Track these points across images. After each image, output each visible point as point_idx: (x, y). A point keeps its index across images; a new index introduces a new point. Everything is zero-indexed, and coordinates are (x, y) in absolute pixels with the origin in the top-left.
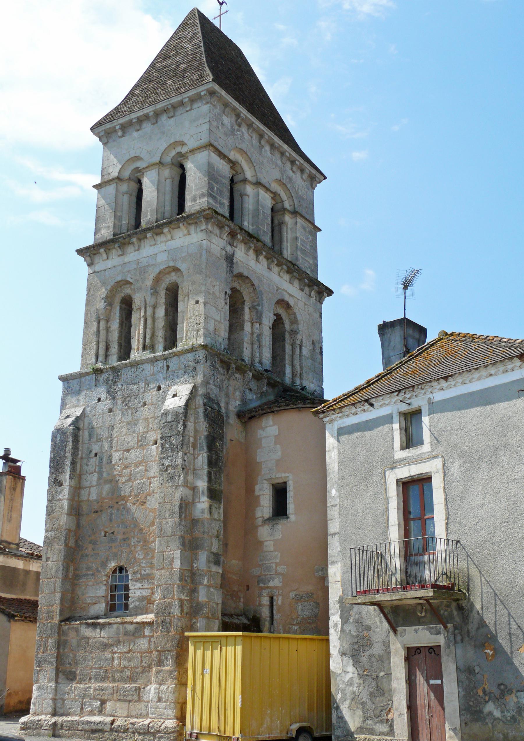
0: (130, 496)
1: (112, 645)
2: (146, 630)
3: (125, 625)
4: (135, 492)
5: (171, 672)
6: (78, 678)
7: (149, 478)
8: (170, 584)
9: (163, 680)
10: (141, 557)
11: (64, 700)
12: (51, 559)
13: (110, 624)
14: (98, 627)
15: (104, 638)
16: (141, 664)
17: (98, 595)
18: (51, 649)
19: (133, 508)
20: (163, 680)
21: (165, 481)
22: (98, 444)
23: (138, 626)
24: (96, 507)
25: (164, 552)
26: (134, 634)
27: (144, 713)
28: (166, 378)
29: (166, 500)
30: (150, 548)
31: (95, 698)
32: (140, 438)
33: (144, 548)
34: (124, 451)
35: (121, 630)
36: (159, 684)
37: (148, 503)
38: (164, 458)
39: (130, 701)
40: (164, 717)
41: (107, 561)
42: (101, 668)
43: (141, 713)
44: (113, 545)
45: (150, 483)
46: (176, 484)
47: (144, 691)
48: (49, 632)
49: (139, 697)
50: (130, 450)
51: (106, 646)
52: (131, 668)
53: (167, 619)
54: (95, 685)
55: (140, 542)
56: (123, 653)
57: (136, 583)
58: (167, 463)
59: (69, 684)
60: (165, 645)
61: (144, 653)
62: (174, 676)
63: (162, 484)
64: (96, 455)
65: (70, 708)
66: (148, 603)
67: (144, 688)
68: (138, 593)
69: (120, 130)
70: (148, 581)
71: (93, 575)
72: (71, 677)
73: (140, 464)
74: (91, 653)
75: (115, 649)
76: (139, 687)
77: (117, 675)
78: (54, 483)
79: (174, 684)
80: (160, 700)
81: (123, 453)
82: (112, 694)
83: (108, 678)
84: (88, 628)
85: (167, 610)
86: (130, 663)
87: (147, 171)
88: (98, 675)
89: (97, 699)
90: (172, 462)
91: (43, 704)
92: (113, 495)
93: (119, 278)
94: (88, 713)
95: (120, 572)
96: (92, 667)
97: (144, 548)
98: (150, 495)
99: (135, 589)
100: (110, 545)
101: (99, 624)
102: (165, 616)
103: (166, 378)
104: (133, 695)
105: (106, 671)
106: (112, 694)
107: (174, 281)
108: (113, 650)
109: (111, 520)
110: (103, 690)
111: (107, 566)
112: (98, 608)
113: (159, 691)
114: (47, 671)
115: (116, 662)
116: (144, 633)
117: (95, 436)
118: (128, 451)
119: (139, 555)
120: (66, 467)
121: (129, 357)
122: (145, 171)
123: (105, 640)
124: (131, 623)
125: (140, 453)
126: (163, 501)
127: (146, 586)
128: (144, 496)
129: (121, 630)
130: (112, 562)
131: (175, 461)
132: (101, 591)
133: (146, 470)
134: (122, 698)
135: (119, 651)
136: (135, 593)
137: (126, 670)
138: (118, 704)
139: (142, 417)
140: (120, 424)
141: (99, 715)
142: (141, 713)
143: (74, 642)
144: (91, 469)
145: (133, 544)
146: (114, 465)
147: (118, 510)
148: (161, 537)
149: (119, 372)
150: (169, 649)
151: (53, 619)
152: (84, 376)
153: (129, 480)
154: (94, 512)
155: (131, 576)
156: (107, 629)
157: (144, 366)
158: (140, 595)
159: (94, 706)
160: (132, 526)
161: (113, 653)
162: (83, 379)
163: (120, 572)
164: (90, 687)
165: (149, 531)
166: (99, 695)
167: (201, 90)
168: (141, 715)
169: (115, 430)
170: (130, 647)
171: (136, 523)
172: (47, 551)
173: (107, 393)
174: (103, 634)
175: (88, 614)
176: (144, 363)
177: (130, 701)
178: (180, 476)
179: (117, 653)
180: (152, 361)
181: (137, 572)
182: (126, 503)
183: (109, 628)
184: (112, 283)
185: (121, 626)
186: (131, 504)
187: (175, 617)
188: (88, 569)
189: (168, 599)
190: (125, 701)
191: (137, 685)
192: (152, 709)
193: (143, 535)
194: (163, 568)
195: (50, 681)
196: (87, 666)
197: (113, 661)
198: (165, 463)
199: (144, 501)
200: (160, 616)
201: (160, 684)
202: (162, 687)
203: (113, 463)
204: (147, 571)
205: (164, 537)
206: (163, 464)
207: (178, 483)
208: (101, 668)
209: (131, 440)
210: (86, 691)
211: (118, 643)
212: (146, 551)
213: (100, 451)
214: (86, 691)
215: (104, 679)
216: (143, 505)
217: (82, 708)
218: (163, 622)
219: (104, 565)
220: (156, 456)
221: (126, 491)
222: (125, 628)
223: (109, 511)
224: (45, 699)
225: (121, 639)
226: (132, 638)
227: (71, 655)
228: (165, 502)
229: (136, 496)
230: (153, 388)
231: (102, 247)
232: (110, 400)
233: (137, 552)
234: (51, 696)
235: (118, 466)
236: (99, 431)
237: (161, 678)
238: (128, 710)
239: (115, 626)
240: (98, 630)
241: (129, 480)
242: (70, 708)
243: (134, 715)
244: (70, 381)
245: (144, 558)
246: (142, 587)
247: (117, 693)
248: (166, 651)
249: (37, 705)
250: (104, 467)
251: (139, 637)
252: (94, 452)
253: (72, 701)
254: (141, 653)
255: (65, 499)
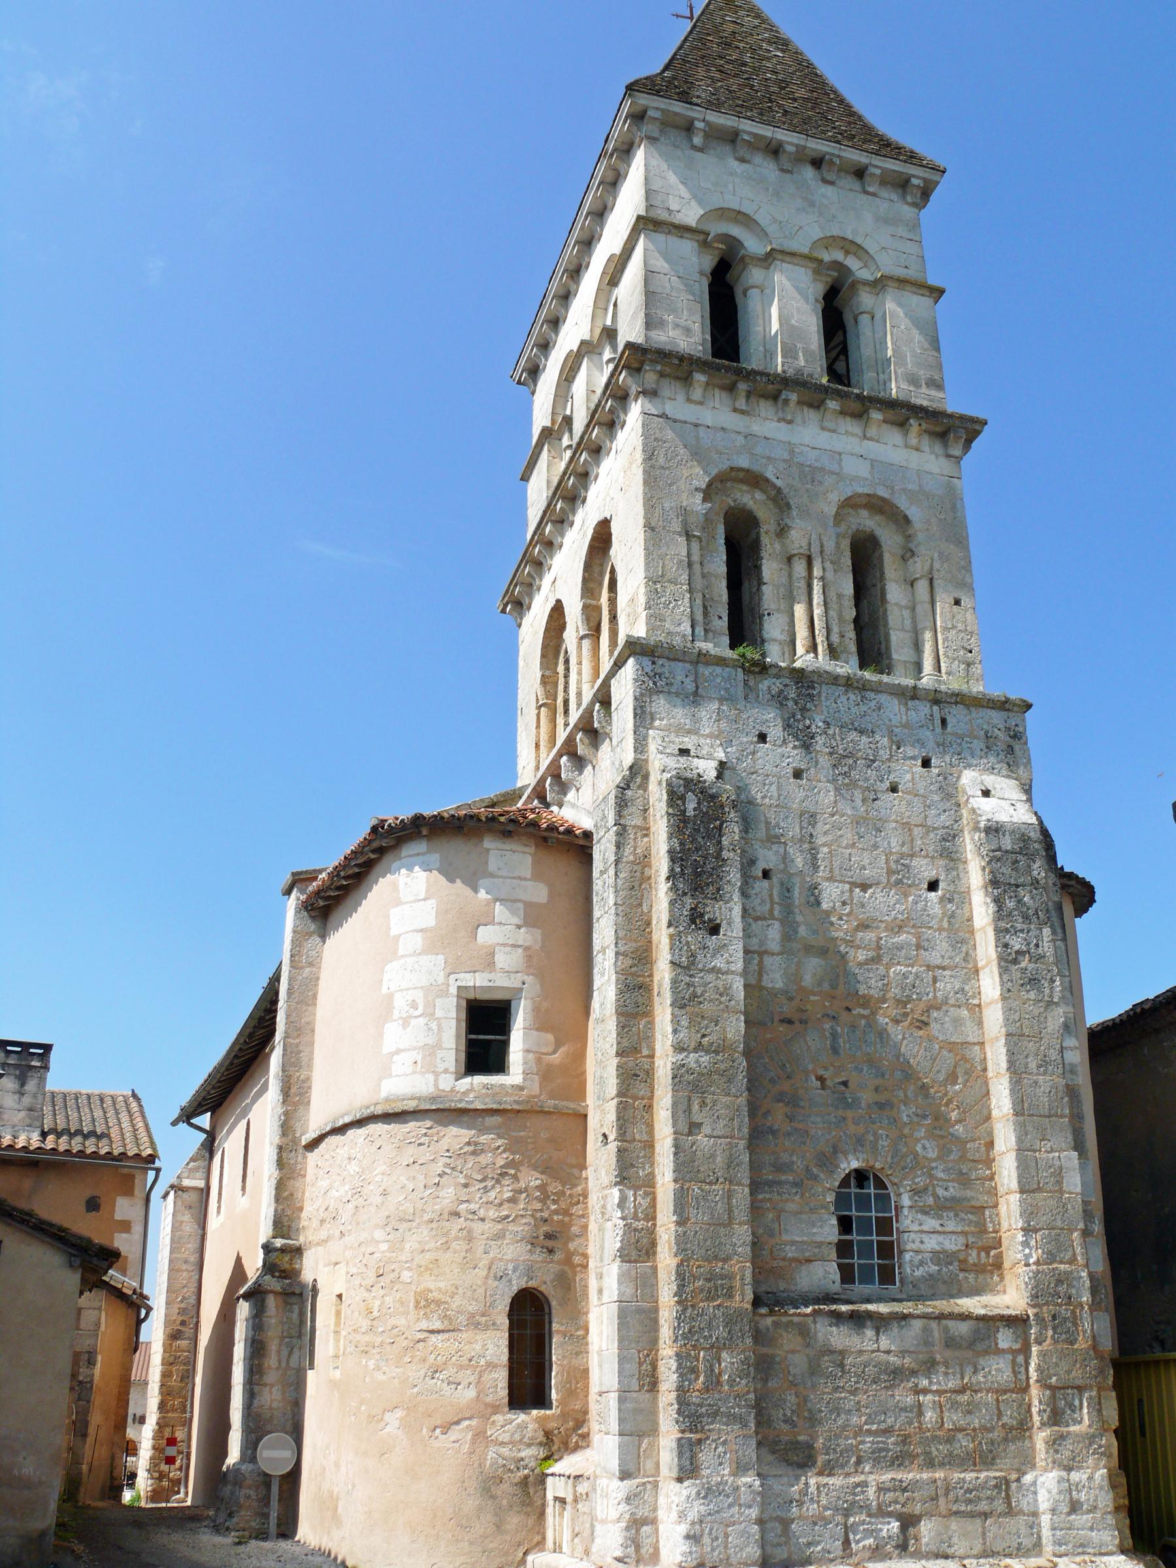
0: (884, 1001)
1: (914, 1373)
2: (1000, 1335)
3: (944, 1322)
4: (894, 991)
5: (1091, 1438)
6: (821, 1459)
7: (929, 967)
8: (1062, 1229)
9: (1073, 1459)
10: (932, 1154)
11: (786, 1523)
12: (706, 1129)
13: (905, 1317)
14: (869, 1323)
15: (888, 1352)
16: (999, 1419)
17: (818, 1239)
18: (731, 1382)
19: (896, 1032)
20: (1073, 1459)
21: (1017, 987)
22: (775, 847)
23: (981, 1324)
24: (787, 1009)
25: (1035, 1151)
26: (971, 1345)
27: (1027, 1542)
28: (943, 744)
29: (1026, 1031)
30: (952, 1135)
31: (882, 1512)
32: (893, 866)
33: (938, 1132)
34: (854, 885)
35: (936, 1334)
36: (1065, 1469)
37: (933, 1024)
38: (1007, 931)
39: (985, 1515)
40: (1090, 1550)
41: (835, 1152)
42: (888, 1431)
43: (1020, 1544)
44: (849, 1114)
45: (935, 980)
46: (1047, 998)
47: (1020, 1488)
48: (721, 1332)
49: (1009, 1504)
50: (870, 886)
51: (896, 1375)
52: (974, 1430)
53: (1065, 1312)
54: (876, 1478)
55: (925, 1117)
56: (946, 1392)
57: (924, 1217)
58: (1017, 944)
59: (798, 1478)
60: (1069, 1372)
61: (1005, 1392)
62: (1100, 1446)
63: (1009, 991)
64: (766, 874)
65: (809, 1544)
66: (962, 1270)
67: (1018, 1480)
68: (932, 1243)
69: (702, 134)
70: (956, 1215)
71: (795, 1184)
72: (798, 1457)
73: (900, 927)
74: (854, 1392)
75: (925, 1383)
76: (1005, 1478)
77: (939, 1450)
78: (693, 921)
79: (1105, 1467)
80: (1075, 1507)
81: (851, 891)
82: (935, 1499)
83: (913, 1457)
84: (837, 1326)
85: (1062, 1289)
86: (969, 1418)
87: (783, 261)
88: (880, 1450)
89: (890, 1514)
90: (1028, 944)
91: (727, 1536)
92: (834, 986)
93: (743, 462)
94: (868, 1554)
95: (860, 1185)
96: (861, 1430)
97: (938, 1132)
98: (938, 1009)
99: (922, 1232)
100: (840, 1112)
101: (870, 1315)
102: (1060, 1305)
103: (943, 744)
104: (991, 1499)
105: (905, 1440)
106: (935, 1499)
107: (868, 530)
108: (916, 1385)
109: (835, 1050)
110: (905, 1490)
111: (837, 1166)
112: (821, 1273)
113: (1070, 1489)
114: (724, 1443)
115: (930, 1416)
116: (997, 1344)
117: (763, 826)
118: (864, 887)
119: (924, 1148)
120: (727, 888)
121: (588, 835)
122: (780, 257)
123: (892, 1359)
124: (965, 1317)
125: (898, 901)
126: (1019, 1031)
127: (951, 1226)
128: (922, 1006)
129: (936, 1334)
130: (850, 1157)
131: (1037, 946)
132: (827, 1229)
133: (919, 947)
134: (963, 1508)
135: (934, 1388)
136: (922, 1242)
137: (960, 1436)
138: (954, 1524)
139: (894, 817)
140: (833, 815)
141: (900, 1557)
142: (1020, 1544)
143: (798, 1363)
144: (758, 908)
145: (905, 1119)
146: (828, 913)
147: (853, 1027)
148: (1023, 1115)
149: (814, 688)
150: (1079, 1382)
151: (730, 1296)
152: (707, 664)
153: (876, 960)
154: (782, 1021)
155: (911, 1198)
156: (896, 1330)
157: (883, 698)
158: (938, 1248)
159: (884, 1533)
160: (898, 1075)
161: (918, 1391)
162: (705, 671)
163: (860, 1185)
164: (864, 1484)
165: (946, 1094)
166: (896, 1502)
167: (747, 128)
168: (1018, 1549)
169: (820, 828)
170: (962, 1378)
171: (908, 1073)
172: (689, 1105)
173: (784, 729)
174: (885, 1342)
175: (793, 1288)
176: (881, 692)
177: (985, 1515)
178: (1052, 981)
179: (930, 1391)
180: (903, 694)
181: (926, 1189)
182: (874, 1013)
183: (902, 1327)
184: (724, 465)
185: (934, 1324)
186: (887, 1020)
187: (1083, 1308)
188: (779, 1168)
189: (1061, 1262)
190: (972, 1515)
191: (998, 1474)
192: (1058, 1533)
193: (930, 1100)
194: (1039, 1189)
195: (740, 1468)
196: (844, 1428)
197: (920, 1414)
198: (1011, 943)
199: (924, 1018)
200: (1047, 1304)
201: (1069, 1469)
202: (1075, 1476)
203: (824, 906)
204: (951, 1190)
205: (1032, 1115)
206: (1006, 946)
207: (1051, 996)
208: (888, 1431)
209: (873, 866)
210: (855, 1494)
211: (930, 1366)
212: (941, 1142)
213: (782, 866)
214: (855, 1494)
215: (900, 1460)
216: (921, 1029)
217: (847, 1543)
218: (1054, 1317)
219: (827, 1161)
220: (941, 920)
221: (870, 984)
222: (946, 1330)
223: (827, 1026)
224: (734, 1524)
225: (938, 1357)
226: (969, 1354)
227: (791, 1399)
228: (1023, 1035)
229: (902, 1003)
230: (913, 758)
231: (704, 372)
232: (795, 747)
233: (918, 1140)
234: (754, 1513)
235: (841, 919)
236: (771, 815)
237: (1068, 1453)
238: (984, 1539)
239: (917, 1324)
240: (870, 1333)
241: (876, 960)
242: (809, 1544)
243: (1000, 1549)
244: (660, 662)
245: (939, 1158)
246: (940, 1229)
247: (946, 1494)
248: (1067, 1388)
249: (706, 1540)
250: (796, 910)
251: (986, 1352)
252: (761, 865)
253: (815, 1524)
254: (997, 1391)
255: (733, 973)
